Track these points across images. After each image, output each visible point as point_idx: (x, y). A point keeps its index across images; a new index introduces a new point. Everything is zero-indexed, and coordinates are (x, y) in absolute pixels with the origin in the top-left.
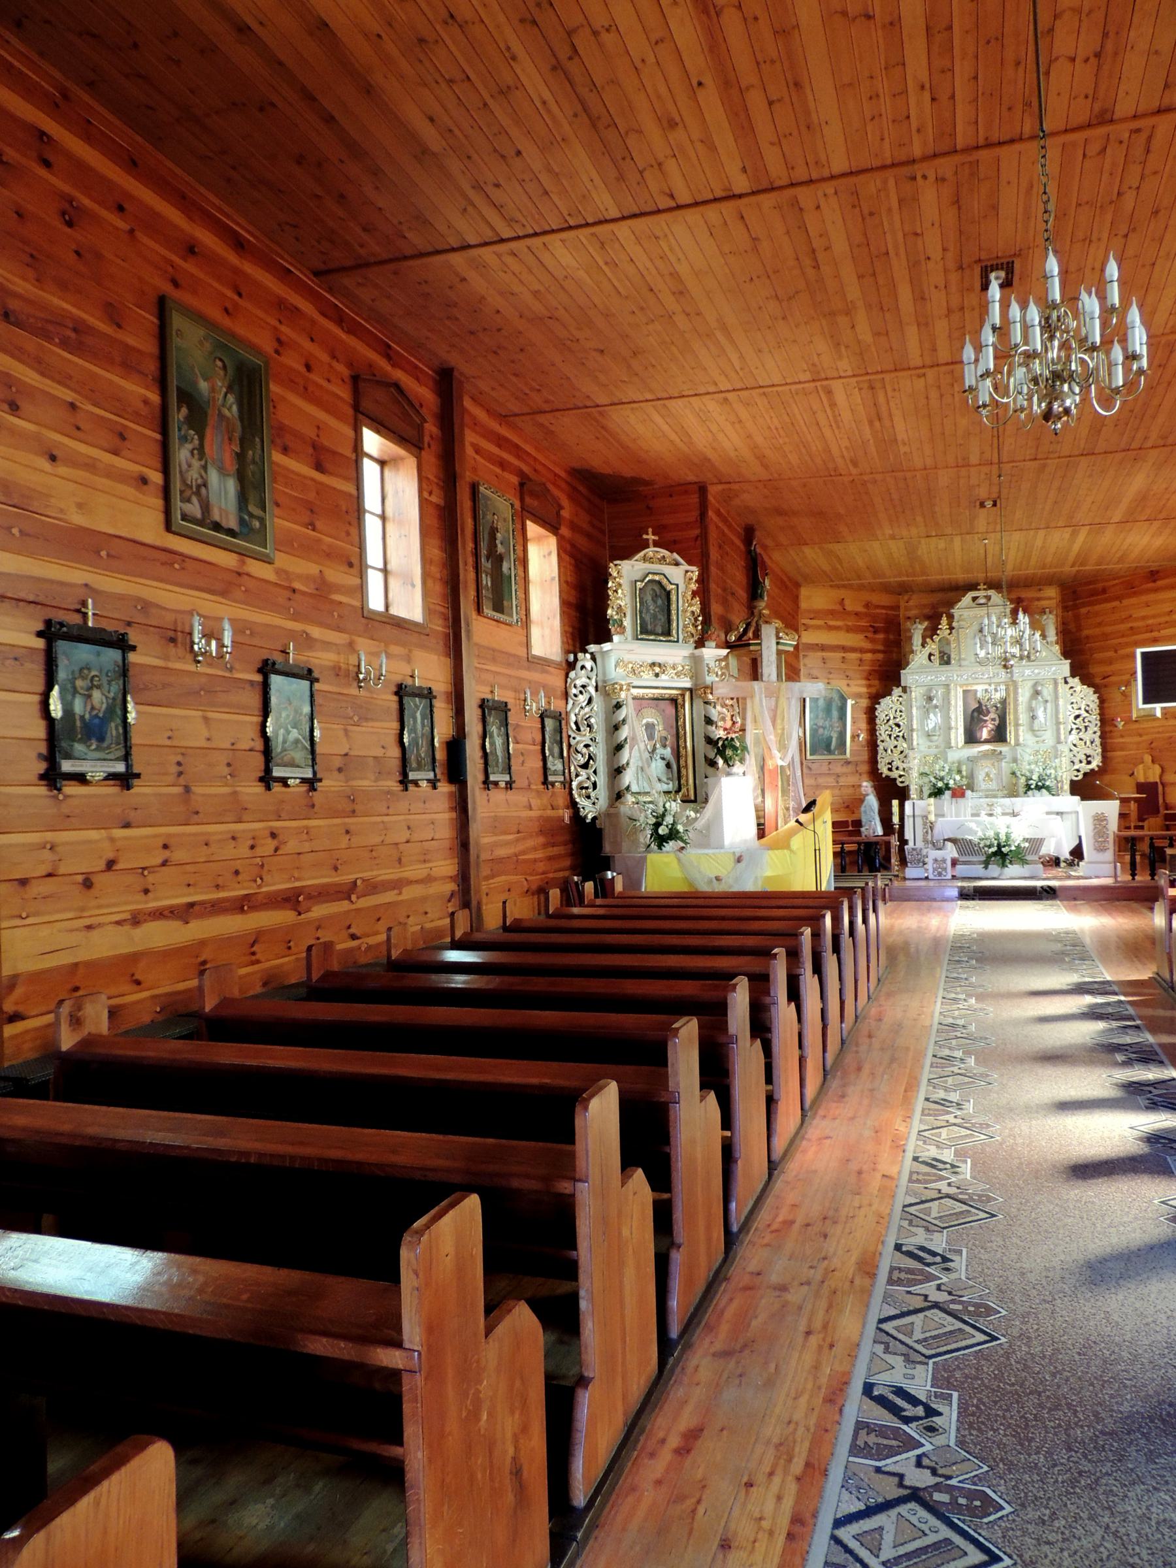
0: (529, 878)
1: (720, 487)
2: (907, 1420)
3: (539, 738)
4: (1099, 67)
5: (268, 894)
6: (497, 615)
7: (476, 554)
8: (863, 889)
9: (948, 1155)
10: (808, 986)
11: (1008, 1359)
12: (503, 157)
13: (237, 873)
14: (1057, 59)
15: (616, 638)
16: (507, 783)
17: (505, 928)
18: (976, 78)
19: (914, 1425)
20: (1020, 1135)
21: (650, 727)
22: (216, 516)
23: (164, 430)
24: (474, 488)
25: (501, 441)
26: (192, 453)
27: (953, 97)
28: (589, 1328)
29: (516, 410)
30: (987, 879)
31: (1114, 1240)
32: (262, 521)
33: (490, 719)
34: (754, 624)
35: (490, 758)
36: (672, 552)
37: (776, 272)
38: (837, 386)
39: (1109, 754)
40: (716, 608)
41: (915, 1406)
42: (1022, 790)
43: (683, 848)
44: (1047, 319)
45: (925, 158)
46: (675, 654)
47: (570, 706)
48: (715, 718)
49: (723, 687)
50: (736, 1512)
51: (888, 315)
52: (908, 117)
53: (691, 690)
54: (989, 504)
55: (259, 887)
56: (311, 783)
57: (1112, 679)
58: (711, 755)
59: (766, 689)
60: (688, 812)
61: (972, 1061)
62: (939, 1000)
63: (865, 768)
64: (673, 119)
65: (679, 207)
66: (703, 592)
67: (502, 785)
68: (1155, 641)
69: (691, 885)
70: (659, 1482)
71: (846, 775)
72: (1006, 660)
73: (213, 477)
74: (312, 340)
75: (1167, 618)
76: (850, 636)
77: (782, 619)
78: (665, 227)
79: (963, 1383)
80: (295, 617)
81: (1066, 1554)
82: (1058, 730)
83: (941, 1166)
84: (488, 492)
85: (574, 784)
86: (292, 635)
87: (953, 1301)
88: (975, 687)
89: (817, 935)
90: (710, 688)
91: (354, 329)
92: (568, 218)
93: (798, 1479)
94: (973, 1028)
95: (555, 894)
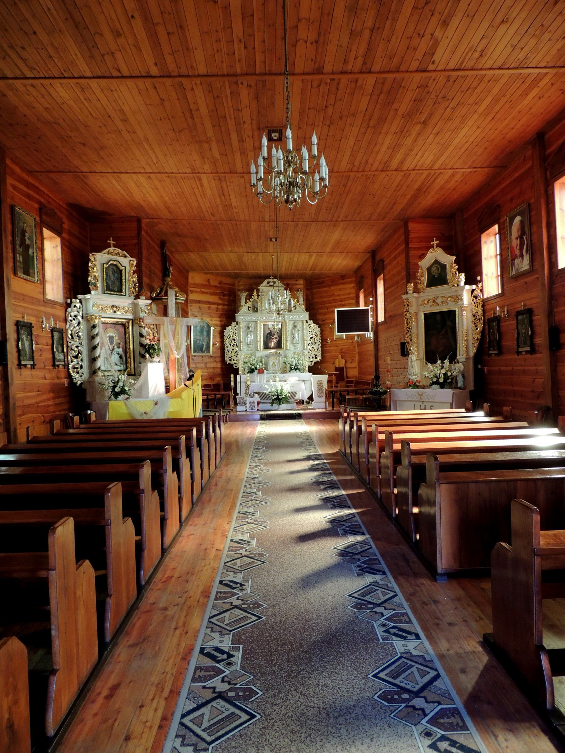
0: (45, 415)
1: (148, 220)
2: (219, 662)
3: (50, 342)
6: (26, 277)
7: (13, 243)
8: (213, 416)
9: (246, 537)
10: (184, 463)
11: (266, 626)
12: (26, 33)
14: (299, 40)
15: (93, 292)
16: (31, 365)
17: (28, 442)
18: (264, 41)
19: (222, 663)
20: (278, 525)
21: (111, 338)
24: (12, 208)
25: (28, 185)
27: (254, 48)
28: (58, 646)
29: (37, 169)
30: (272, 410)
31: (314, 567)
34: (165, 289)
35: (22, 352)
37: (173, 117)
38: (204, 178)
39: (325, 354)
40: (145, 280)
41: (223, 654)
42: (288, 370)
43: (128, 398)
44: (287, 157)
45: (242, 75)
47: (68, 326)
48: (144, 334)
49: (149, 320)
50: (134, 721)
51: (226, 146)
52: (234, 54)
53: (132, 320)
54: (274, 240)
57: (326, 321)
58: (143, 352)
59: (170, 320)
60: (130, 381)
61: (260, 493)
62: (248, 466)
63: (219, 359)
64: (119, 32)
65: (123, 77)
66: (139, 271)
67: (29, 366)
68: (343, 306)
69: (132, 417)
70: (95, 715)
71: (210, 362)
72: (279, 311)
75: (348, 296)
76: (212, 296)
77: (178, 287)
78: (116, 87)
79: (245, 640)
81: (283, 708)
82: (304, 343)
83: (243, 542)
84: (21, 211)
85: (70, 366)
87: (243, 604)
88: (268, 323)
89: (189, 439)
90: (142, 319)
92: (63, 72)
93: (166, 699)
94: (261, 478)
95: (57, 423)
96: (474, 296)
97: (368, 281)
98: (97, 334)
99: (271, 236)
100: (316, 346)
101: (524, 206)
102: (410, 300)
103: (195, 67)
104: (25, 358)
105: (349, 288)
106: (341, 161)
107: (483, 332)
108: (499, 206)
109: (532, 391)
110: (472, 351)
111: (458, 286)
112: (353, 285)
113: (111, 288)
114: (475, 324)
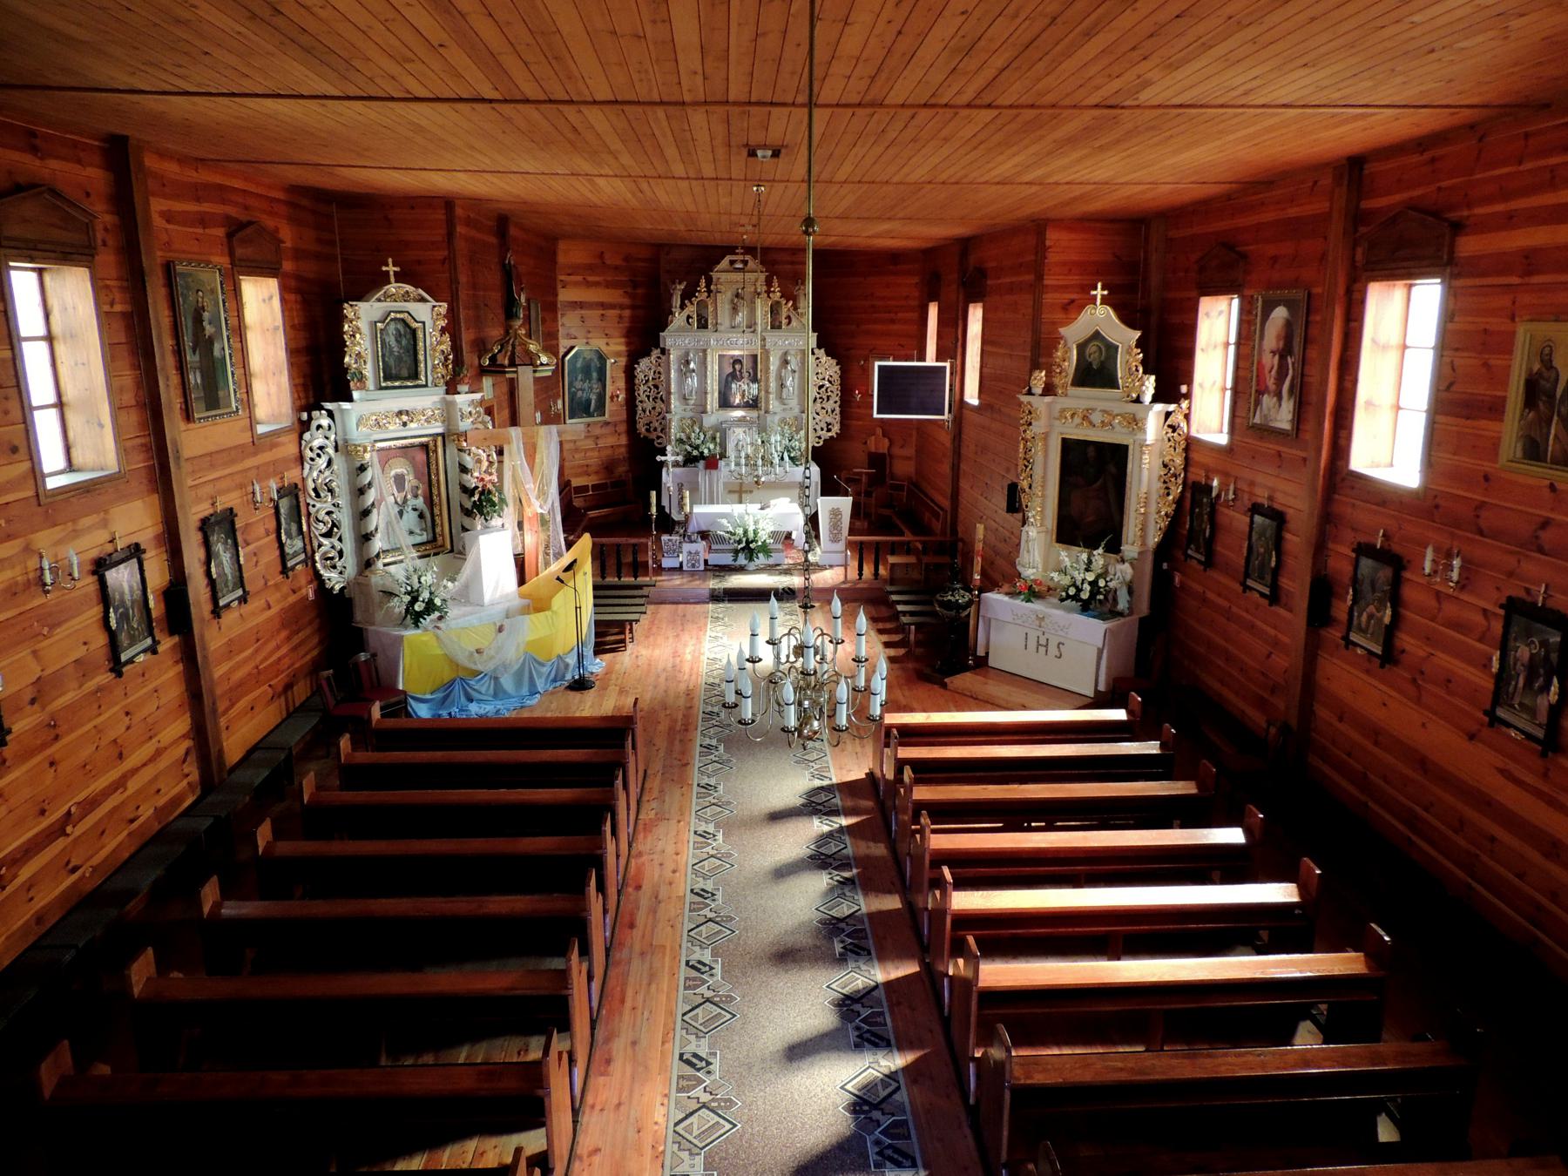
3: (272, 525)
7: (179, 353)
15: (356, 395)
21: (399, 480)
24: (168, 268)
33: (214, 538)
35: (219, 585)
36: (416, 287)
46: (425, 400)
53: (443, 435)
63: (622, 428)
66: (452, 329)
96: (1169, 426)
98: (370, 484)
100: (829, 405)
107: (1179, 502)
110: (1154, 539)
112: (916, 280)
113: (394, 372)
114: (1165, 482)
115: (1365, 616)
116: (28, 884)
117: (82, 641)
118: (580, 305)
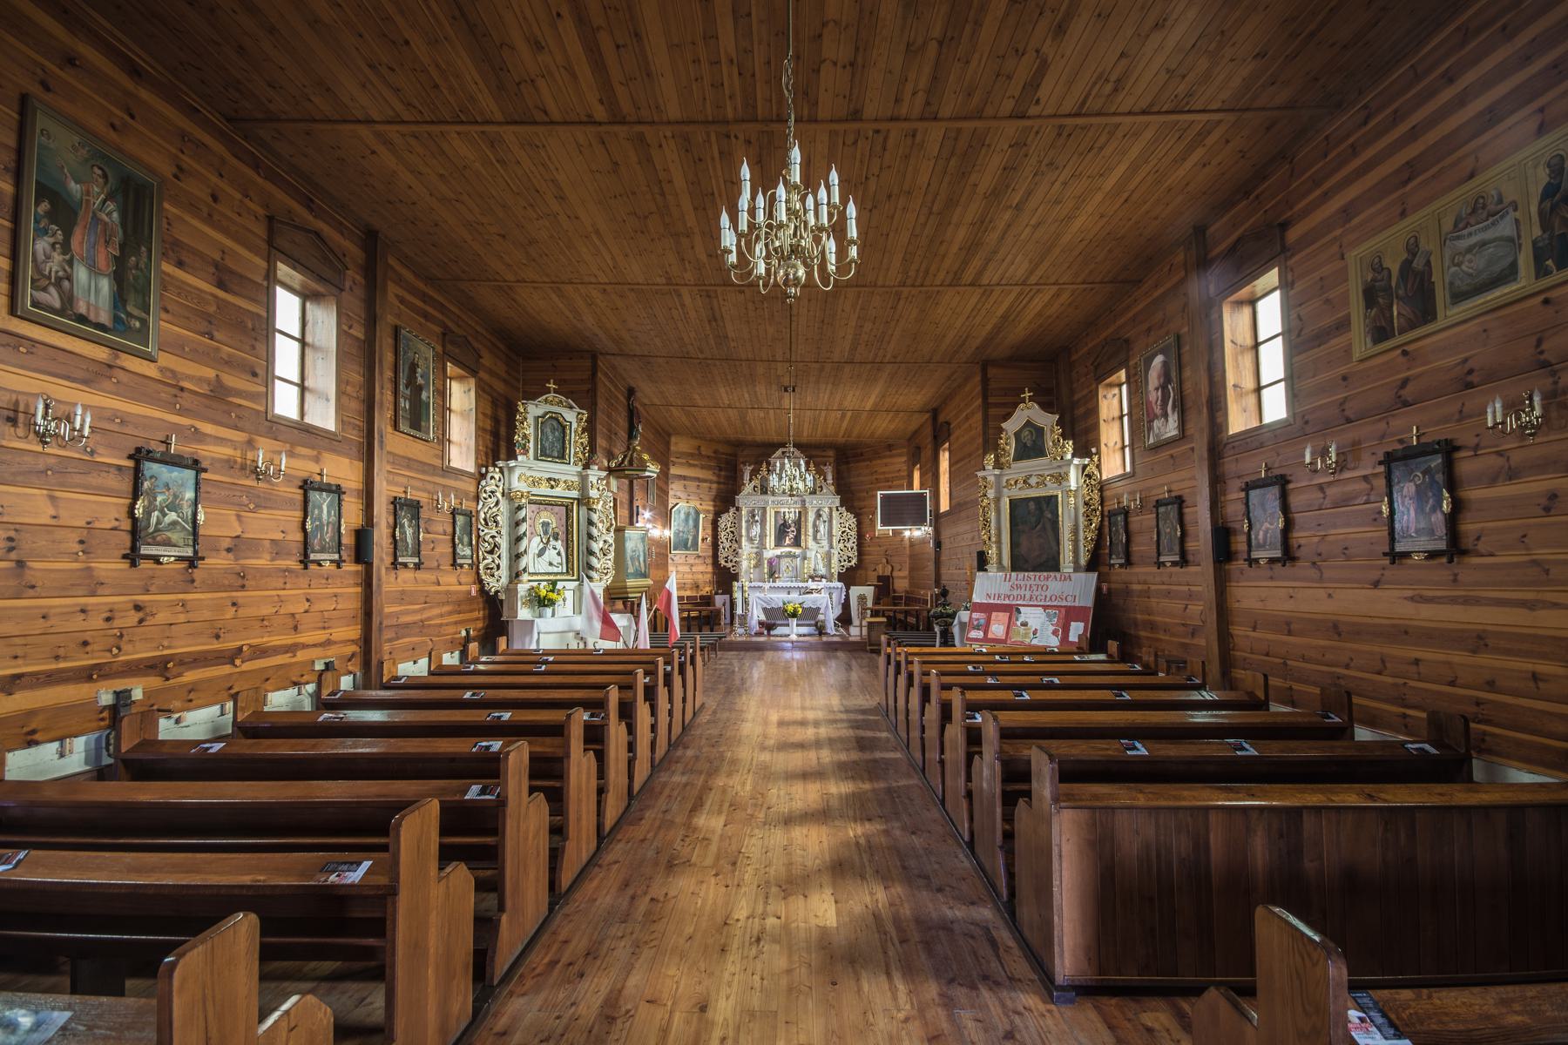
3: (449, 530)
4: (853, 75)
5: (127, 663)
6: (413, 432)
13: (85, 643)
14: (825, 60)
15: (520, 458)
21: (546, 525)
22: (82, 308)
23: (16, 218)
25: (424, 297)
26: (53, 246)
32: (145, 323)
35: (399, 544)
38: (685, 291)
46: (568, 472)
52: (722, 85)
53: (578, 499)
55: (115, 656)
56: (192, 562)
63: (709, 561)
65: (552, 123)
66: (590, 428)
68: (890, 488)
73: (81, 274)
74: (221, 175)
76: (704, 471)
80: (180, 413)
85: (481, 567)
86: (177, 428)
91: (272, 177)
97: (927, 453)
98: (524, 520)
99: (787, 384)
101: (1171, 340)
102: (989, 478)
103: (663, 108)
104: (405, 553)
105: (899, 462)
106: (888, 269)
107: (1100, 529)
108: (1127, 341)
109: (1183, 625)
111: (1062, 459)
115: (1261, 533)
116: (190, 687)
117: (282, 529)
118: (684, 478)
